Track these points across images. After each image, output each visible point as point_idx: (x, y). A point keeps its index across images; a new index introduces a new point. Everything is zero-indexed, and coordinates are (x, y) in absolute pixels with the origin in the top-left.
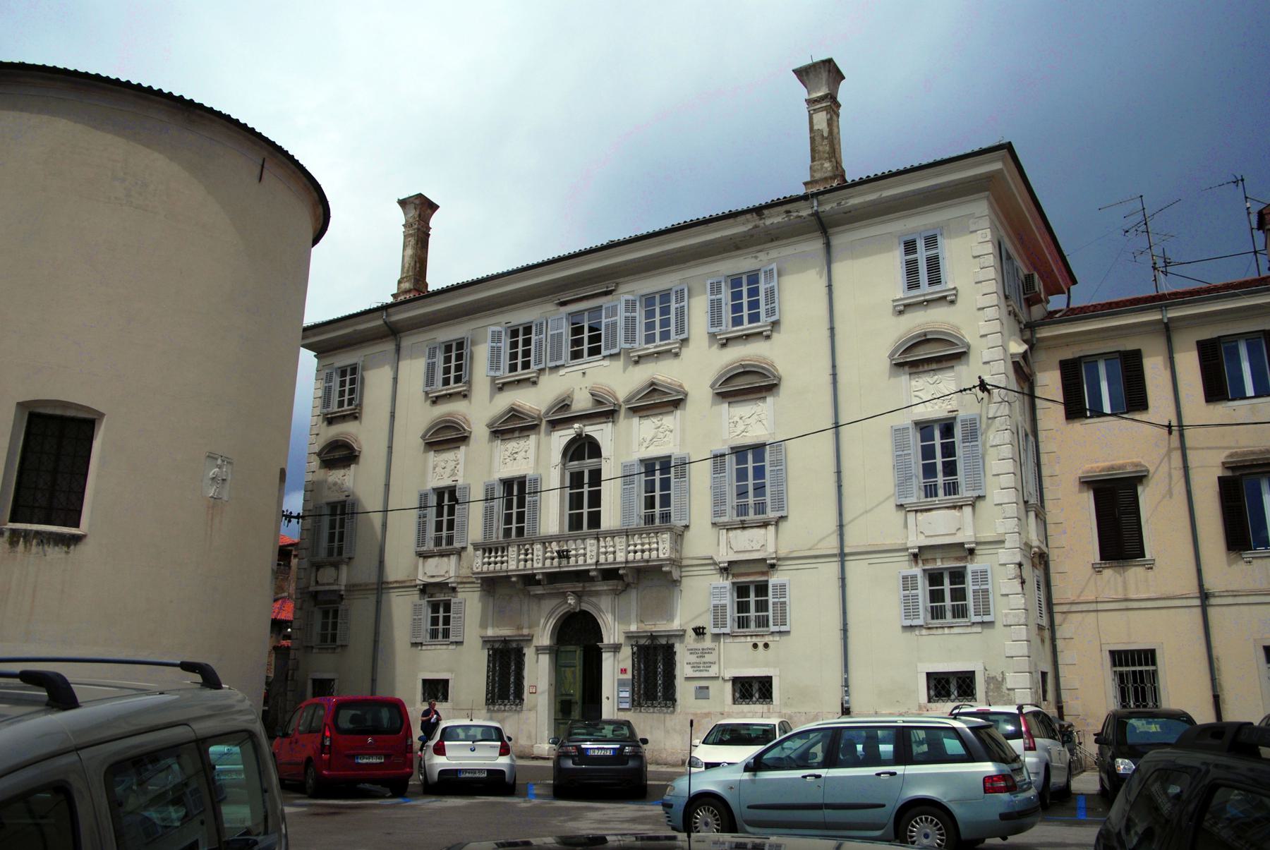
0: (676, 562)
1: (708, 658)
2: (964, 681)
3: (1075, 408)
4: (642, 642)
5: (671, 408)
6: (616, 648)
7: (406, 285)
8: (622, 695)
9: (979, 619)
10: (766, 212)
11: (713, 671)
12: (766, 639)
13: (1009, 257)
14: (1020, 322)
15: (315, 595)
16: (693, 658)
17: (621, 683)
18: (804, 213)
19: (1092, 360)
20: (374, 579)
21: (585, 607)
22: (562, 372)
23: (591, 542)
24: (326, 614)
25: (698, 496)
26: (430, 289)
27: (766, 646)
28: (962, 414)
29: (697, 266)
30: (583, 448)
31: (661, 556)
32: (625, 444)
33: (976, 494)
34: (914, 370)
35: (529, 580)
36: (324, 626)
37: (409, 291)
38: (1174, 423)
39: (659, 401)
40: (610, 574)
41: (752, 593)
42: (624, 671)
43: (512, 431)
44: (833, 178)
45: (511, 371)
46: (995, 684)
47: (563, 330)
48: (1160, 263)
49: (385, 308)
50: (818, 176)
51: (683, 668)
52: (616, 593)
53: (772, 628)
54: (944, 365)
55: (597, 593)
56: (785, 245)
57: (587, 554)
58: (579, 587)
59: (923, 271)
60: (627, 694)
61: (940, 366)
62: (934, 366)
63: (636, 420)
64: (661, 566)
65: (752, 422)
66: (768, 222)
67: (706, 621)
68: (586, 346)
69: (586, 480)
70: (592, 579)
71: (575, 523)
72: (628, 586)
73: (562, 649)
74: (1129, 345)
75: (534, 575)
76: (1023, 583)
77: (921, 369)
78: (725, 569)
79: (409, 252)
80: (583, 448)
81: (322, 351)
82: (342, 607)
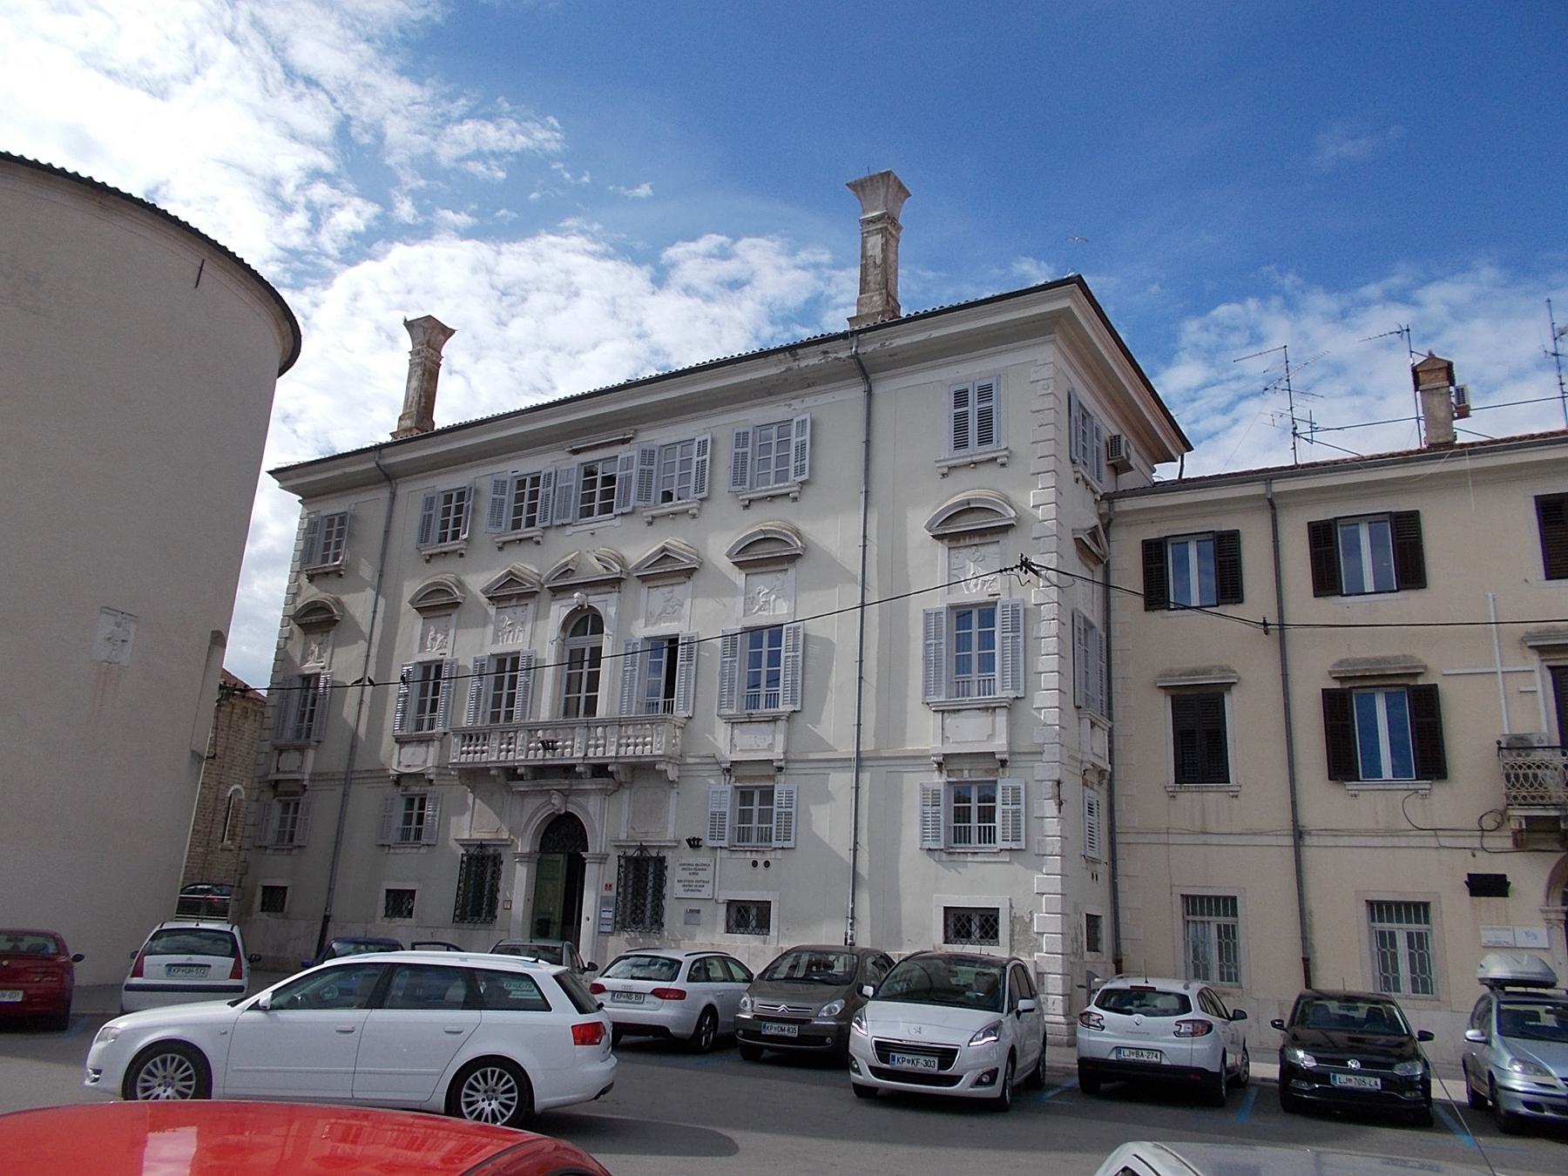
0: (679, 760)
1: (702, 876)
2: (987, 920)
3: (1156, 596)
4: (630, 853)
5: (682, 579)
6: (602, 859)
7: (408, 423)
8: (605, 915)
9: (1008, 845)
10: (800, 351)
11: (706, 892)
12: (768, 857)
13: (1086, 415)
14: (1095, 493)
15: (275, 784)
16: (685, 875)
17: (604, 902)
18: (843, 355)
19: (1182, 540)
20: (342, 767)
21: (572, 809)
22: (569, 530)
23: (580, 733)
24: (286, 806)
25: (708, 685)
26: (438, 426)
27: (767, 864)
28: (1004, 598)
29: (723, 413)
30: (585, 622)
31: (656, 752)
32: (634, 621)
33: (1012, 695)
34: (954, 544)
35: (511, 773)
36: (283, 821)
37: (411, 429)
38: (1272, 619)
39: (669, 571)
40: (600, 770)
41: (757, 799)
42: (608, 887)
43: (509, 598)
44: (883, 313)
45: (513, 528)
46: (1021, 925)
47: (574, 483)
48: (1303, 428)
49: (379, 448)
50: (865, 310)
51: (674, 888)
52: (607, 793)
53: (775, 844)
54: (988, 539)
55: (585, 792)
56: (821, 392)
57: (574, 749)
58: (564, 784)
59: (974, 422)
60: (610, 915)
61: (984, 540)
62: (977, 541)
63: (644, 591)
64: (654, 763)
65: (773, 602)
66: (803, 364)
67: (701, 830)
68: (597, 503)
69: (587, 657)
70: (579, 776)
71: (569, 709)
72: (621, 784)
73: (546, 857)
74: (1226, 525)
75: (516, 768)
76: (1060, 804)
77: (962, 543)
78: (728, 770)
79: (414, 384)
80: (585, 622)
81: (308, 495)
82: (302, 800)
